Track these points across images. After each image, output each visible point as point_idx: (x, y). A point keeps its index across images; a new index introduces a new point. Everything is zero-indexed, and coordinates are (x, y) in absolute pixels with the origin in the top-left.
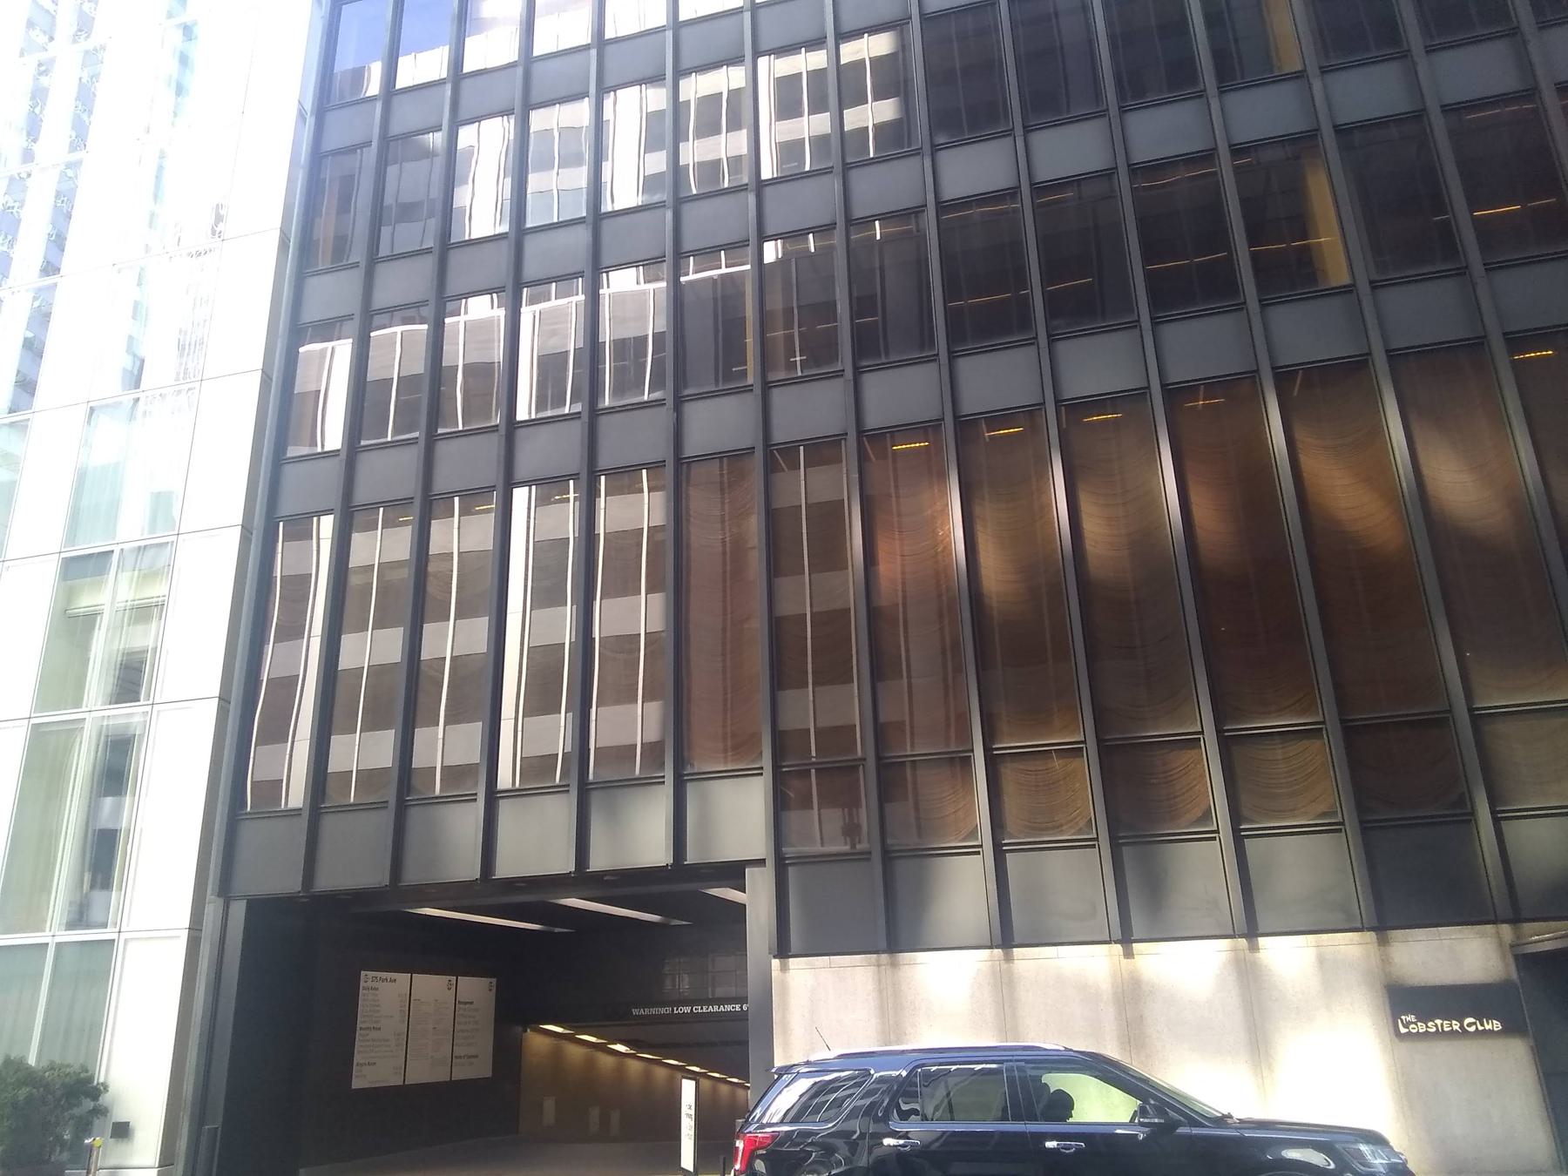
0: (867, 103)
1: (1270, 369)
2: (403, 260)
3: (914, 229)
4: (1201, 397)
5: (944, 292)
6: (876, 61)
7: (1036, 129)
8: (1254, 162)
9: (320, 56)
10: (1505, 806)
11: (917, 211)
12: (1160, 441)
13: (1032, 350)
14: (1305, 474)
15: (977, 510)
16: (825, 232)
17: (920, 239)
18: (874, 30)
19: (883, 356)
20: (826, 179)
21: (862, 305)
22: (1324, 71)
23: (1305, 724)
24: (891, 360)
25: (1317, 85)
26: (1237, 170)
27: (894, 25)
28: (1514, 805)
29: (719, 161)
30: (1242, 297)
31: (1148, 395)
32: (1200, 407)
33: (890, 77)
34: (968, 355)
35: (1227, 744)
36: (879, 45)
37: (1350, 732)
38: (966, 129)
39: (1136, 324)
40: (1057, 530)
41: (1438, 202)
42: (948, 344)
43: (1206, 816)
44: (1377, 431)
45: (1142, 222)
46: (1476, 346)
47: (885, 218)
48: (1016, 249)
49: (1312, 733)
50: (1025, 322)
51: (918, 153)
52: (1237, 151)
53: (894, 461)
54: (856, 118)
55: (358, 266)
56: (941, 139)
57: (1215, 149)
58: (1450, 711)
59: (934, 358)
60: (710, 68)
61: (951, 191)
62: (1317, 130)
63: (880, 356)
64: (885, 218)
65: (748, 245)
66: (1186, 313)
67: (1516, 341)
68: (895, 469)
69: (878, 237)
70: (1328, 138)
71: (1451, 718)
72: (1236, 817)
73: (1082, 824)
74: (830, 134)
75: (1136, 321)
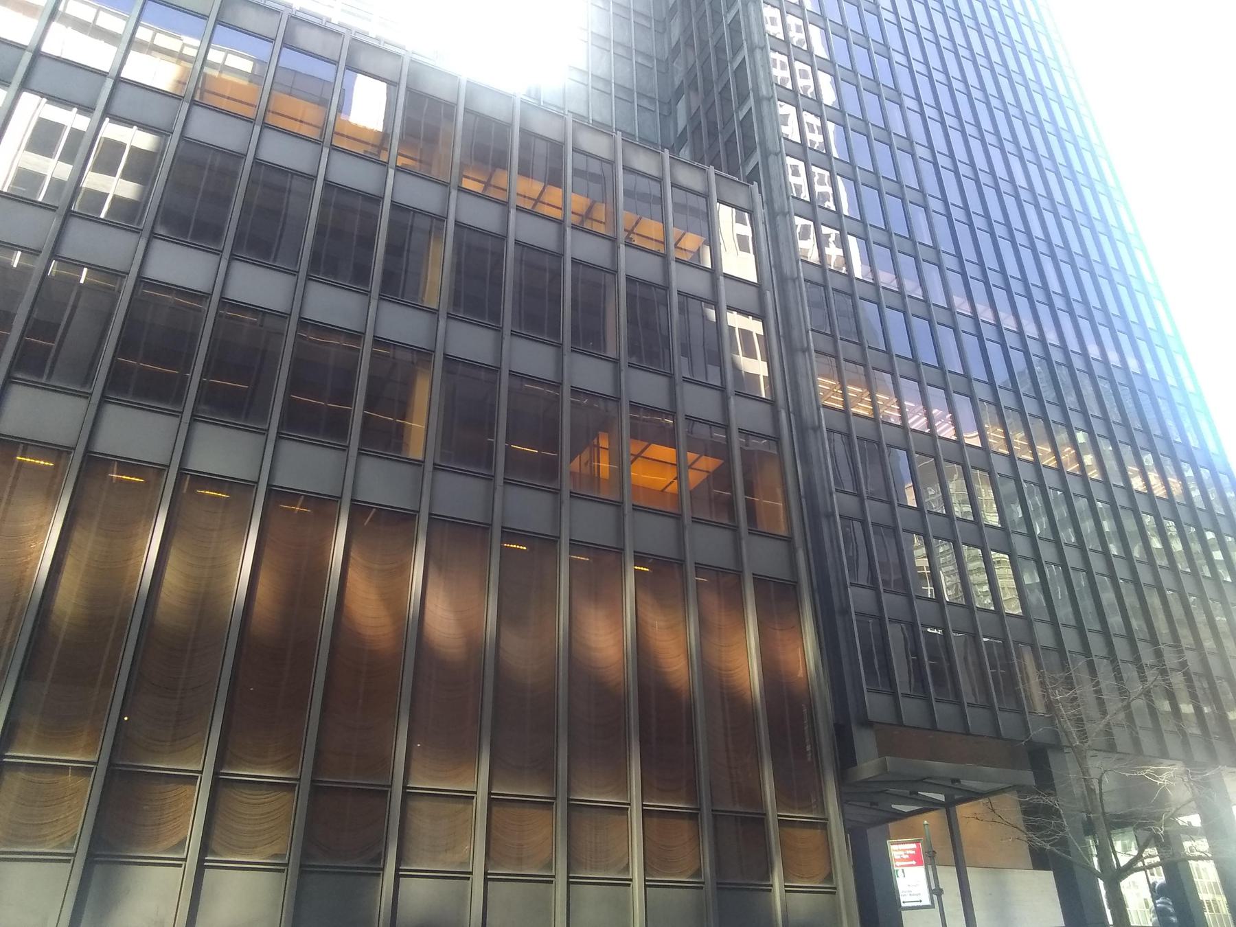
0: (115, 176)
1: (349, 500)
2: (123, 231)
3: (116, 289)
4: (300, 504)
5: (117, 345)
6: (134, 150)
7: (160, 238)
8: (391, 356)
9: (351, 100)
10: (407, 866)
11: (120, 275)
12: (251, 527)
13: (176, 421)
14: (348, 584)
15: (77, 536)
16: (97, 272)
17: (114, 297)
18: (144, 127)
19: (45, 377)
20: (49, 214)
21: (34, 327)
22: (450, 316)
23: (814, 818)
24: (51, 383)
25: (442, 323)
26: (374, 355)
27: (161, 132)
28: (580, 874)
29: (43, 177)
30: (348, 442)
31: (166, 472)
32: (296, 512)
33: (142, 165)
34: (214, 424)
35: (218, 783)
36: (145, 141)
37: (317, 790)
38: (245, 246)
39: (265, 432)
40: (140, 576)
41: (489, 427)
42: (104, 387)
43: (181, 845)
44: (403, 569)
45: (296, 362)
46: (486, 528)
47: (91, 267)
48: (192, 338)
49: (288, 787)
50: (179, 398)
51: (137, 231)
52: (377, 341)
53: (18, 471)
54: (93, 180)
55: (55, 211)
56: (161, 231)
57: (364, 334)
58: (390, 786)
59: (87, 396)
60: (126, 122)
61: (153, 272)
62: (363, 334)
63: (40, 375)
64: (91, 267)
65: (38, 255)
66: (211, 419)
67: (509, 534)
68: (16, 478)
69: (82, 281)
70: (439, 359)
71: (199, 777)
72: (205, 848)
73: (66, 838)
74: (65, 182)
75: (266, 430)
